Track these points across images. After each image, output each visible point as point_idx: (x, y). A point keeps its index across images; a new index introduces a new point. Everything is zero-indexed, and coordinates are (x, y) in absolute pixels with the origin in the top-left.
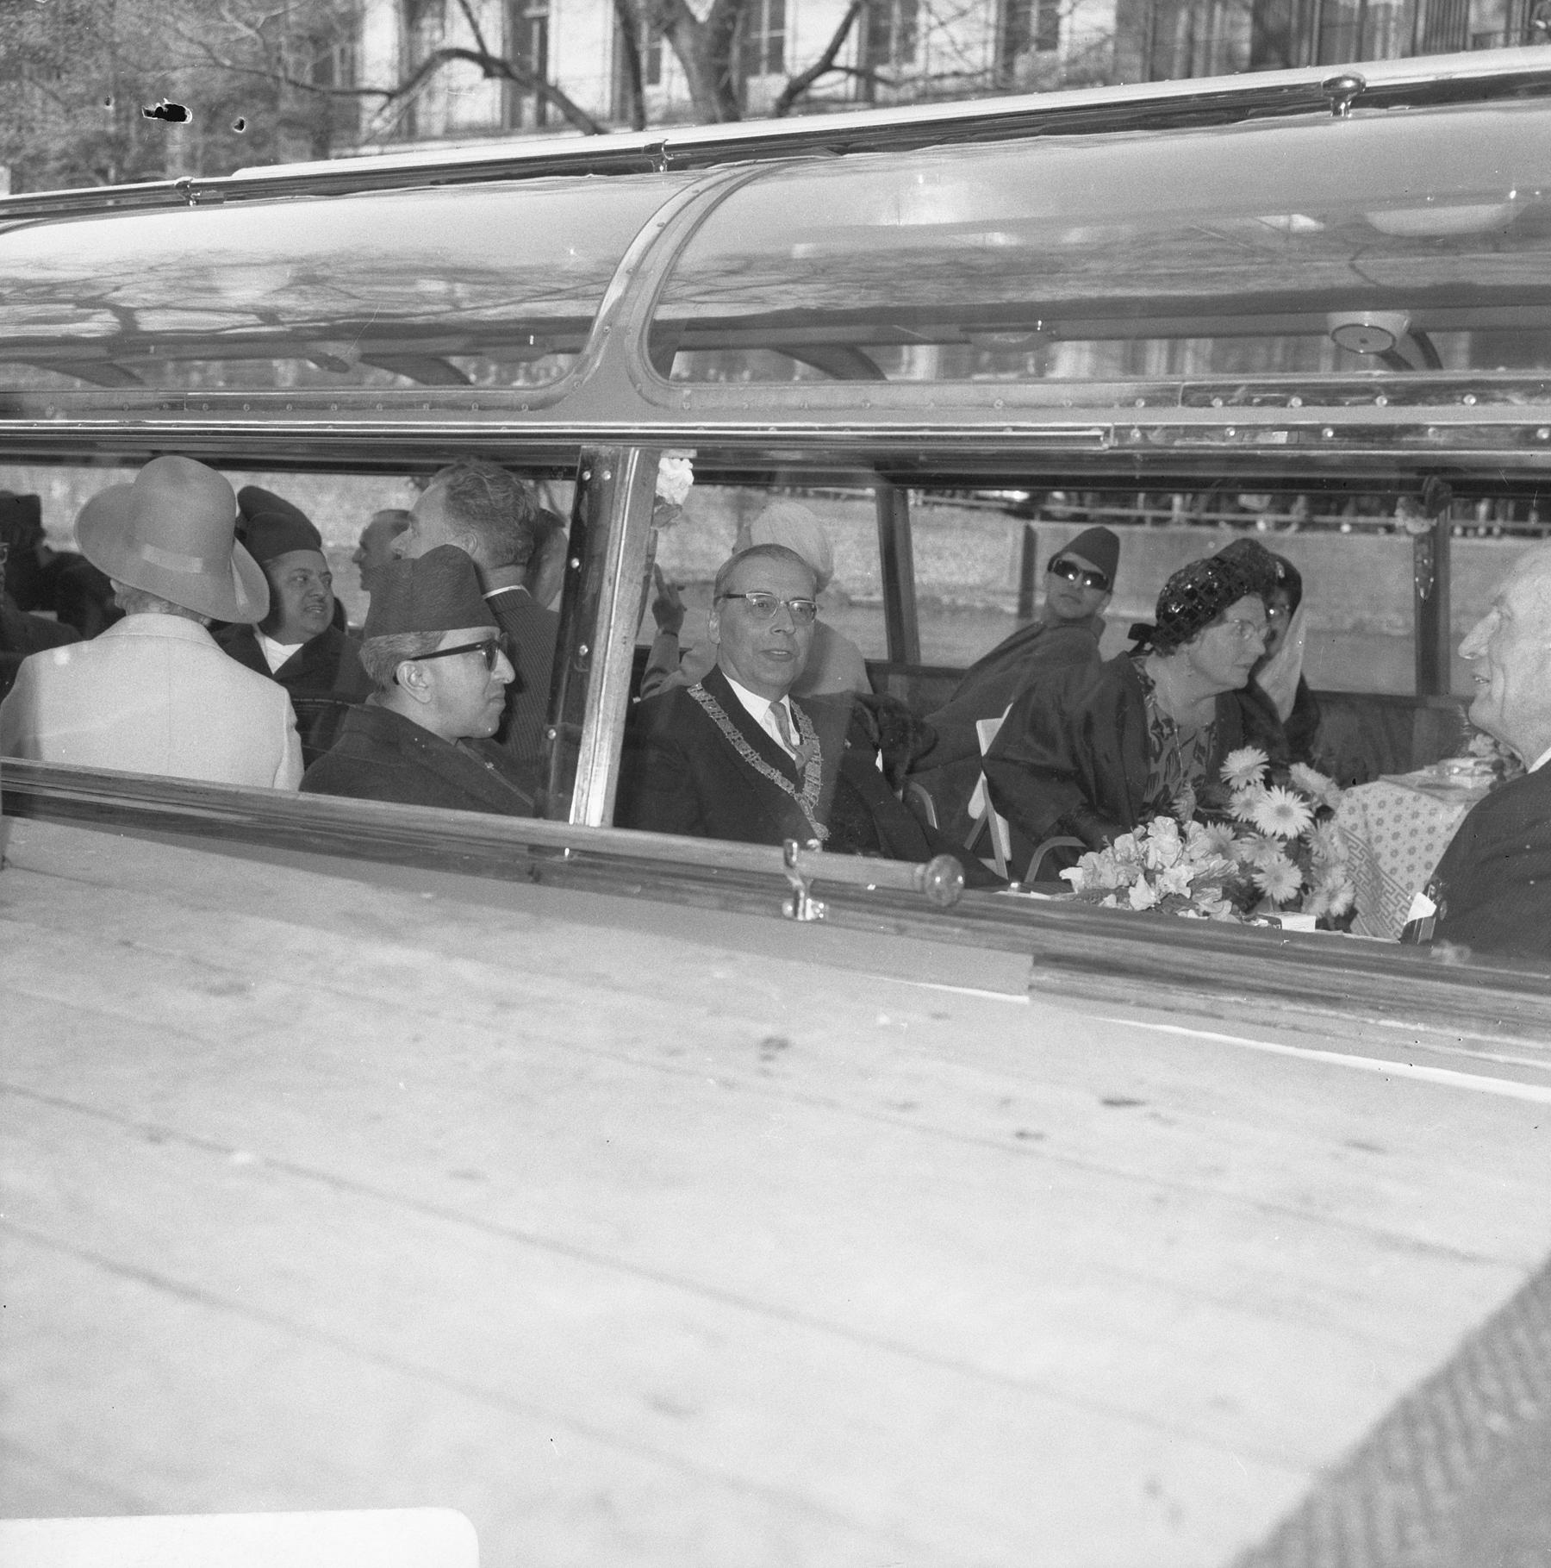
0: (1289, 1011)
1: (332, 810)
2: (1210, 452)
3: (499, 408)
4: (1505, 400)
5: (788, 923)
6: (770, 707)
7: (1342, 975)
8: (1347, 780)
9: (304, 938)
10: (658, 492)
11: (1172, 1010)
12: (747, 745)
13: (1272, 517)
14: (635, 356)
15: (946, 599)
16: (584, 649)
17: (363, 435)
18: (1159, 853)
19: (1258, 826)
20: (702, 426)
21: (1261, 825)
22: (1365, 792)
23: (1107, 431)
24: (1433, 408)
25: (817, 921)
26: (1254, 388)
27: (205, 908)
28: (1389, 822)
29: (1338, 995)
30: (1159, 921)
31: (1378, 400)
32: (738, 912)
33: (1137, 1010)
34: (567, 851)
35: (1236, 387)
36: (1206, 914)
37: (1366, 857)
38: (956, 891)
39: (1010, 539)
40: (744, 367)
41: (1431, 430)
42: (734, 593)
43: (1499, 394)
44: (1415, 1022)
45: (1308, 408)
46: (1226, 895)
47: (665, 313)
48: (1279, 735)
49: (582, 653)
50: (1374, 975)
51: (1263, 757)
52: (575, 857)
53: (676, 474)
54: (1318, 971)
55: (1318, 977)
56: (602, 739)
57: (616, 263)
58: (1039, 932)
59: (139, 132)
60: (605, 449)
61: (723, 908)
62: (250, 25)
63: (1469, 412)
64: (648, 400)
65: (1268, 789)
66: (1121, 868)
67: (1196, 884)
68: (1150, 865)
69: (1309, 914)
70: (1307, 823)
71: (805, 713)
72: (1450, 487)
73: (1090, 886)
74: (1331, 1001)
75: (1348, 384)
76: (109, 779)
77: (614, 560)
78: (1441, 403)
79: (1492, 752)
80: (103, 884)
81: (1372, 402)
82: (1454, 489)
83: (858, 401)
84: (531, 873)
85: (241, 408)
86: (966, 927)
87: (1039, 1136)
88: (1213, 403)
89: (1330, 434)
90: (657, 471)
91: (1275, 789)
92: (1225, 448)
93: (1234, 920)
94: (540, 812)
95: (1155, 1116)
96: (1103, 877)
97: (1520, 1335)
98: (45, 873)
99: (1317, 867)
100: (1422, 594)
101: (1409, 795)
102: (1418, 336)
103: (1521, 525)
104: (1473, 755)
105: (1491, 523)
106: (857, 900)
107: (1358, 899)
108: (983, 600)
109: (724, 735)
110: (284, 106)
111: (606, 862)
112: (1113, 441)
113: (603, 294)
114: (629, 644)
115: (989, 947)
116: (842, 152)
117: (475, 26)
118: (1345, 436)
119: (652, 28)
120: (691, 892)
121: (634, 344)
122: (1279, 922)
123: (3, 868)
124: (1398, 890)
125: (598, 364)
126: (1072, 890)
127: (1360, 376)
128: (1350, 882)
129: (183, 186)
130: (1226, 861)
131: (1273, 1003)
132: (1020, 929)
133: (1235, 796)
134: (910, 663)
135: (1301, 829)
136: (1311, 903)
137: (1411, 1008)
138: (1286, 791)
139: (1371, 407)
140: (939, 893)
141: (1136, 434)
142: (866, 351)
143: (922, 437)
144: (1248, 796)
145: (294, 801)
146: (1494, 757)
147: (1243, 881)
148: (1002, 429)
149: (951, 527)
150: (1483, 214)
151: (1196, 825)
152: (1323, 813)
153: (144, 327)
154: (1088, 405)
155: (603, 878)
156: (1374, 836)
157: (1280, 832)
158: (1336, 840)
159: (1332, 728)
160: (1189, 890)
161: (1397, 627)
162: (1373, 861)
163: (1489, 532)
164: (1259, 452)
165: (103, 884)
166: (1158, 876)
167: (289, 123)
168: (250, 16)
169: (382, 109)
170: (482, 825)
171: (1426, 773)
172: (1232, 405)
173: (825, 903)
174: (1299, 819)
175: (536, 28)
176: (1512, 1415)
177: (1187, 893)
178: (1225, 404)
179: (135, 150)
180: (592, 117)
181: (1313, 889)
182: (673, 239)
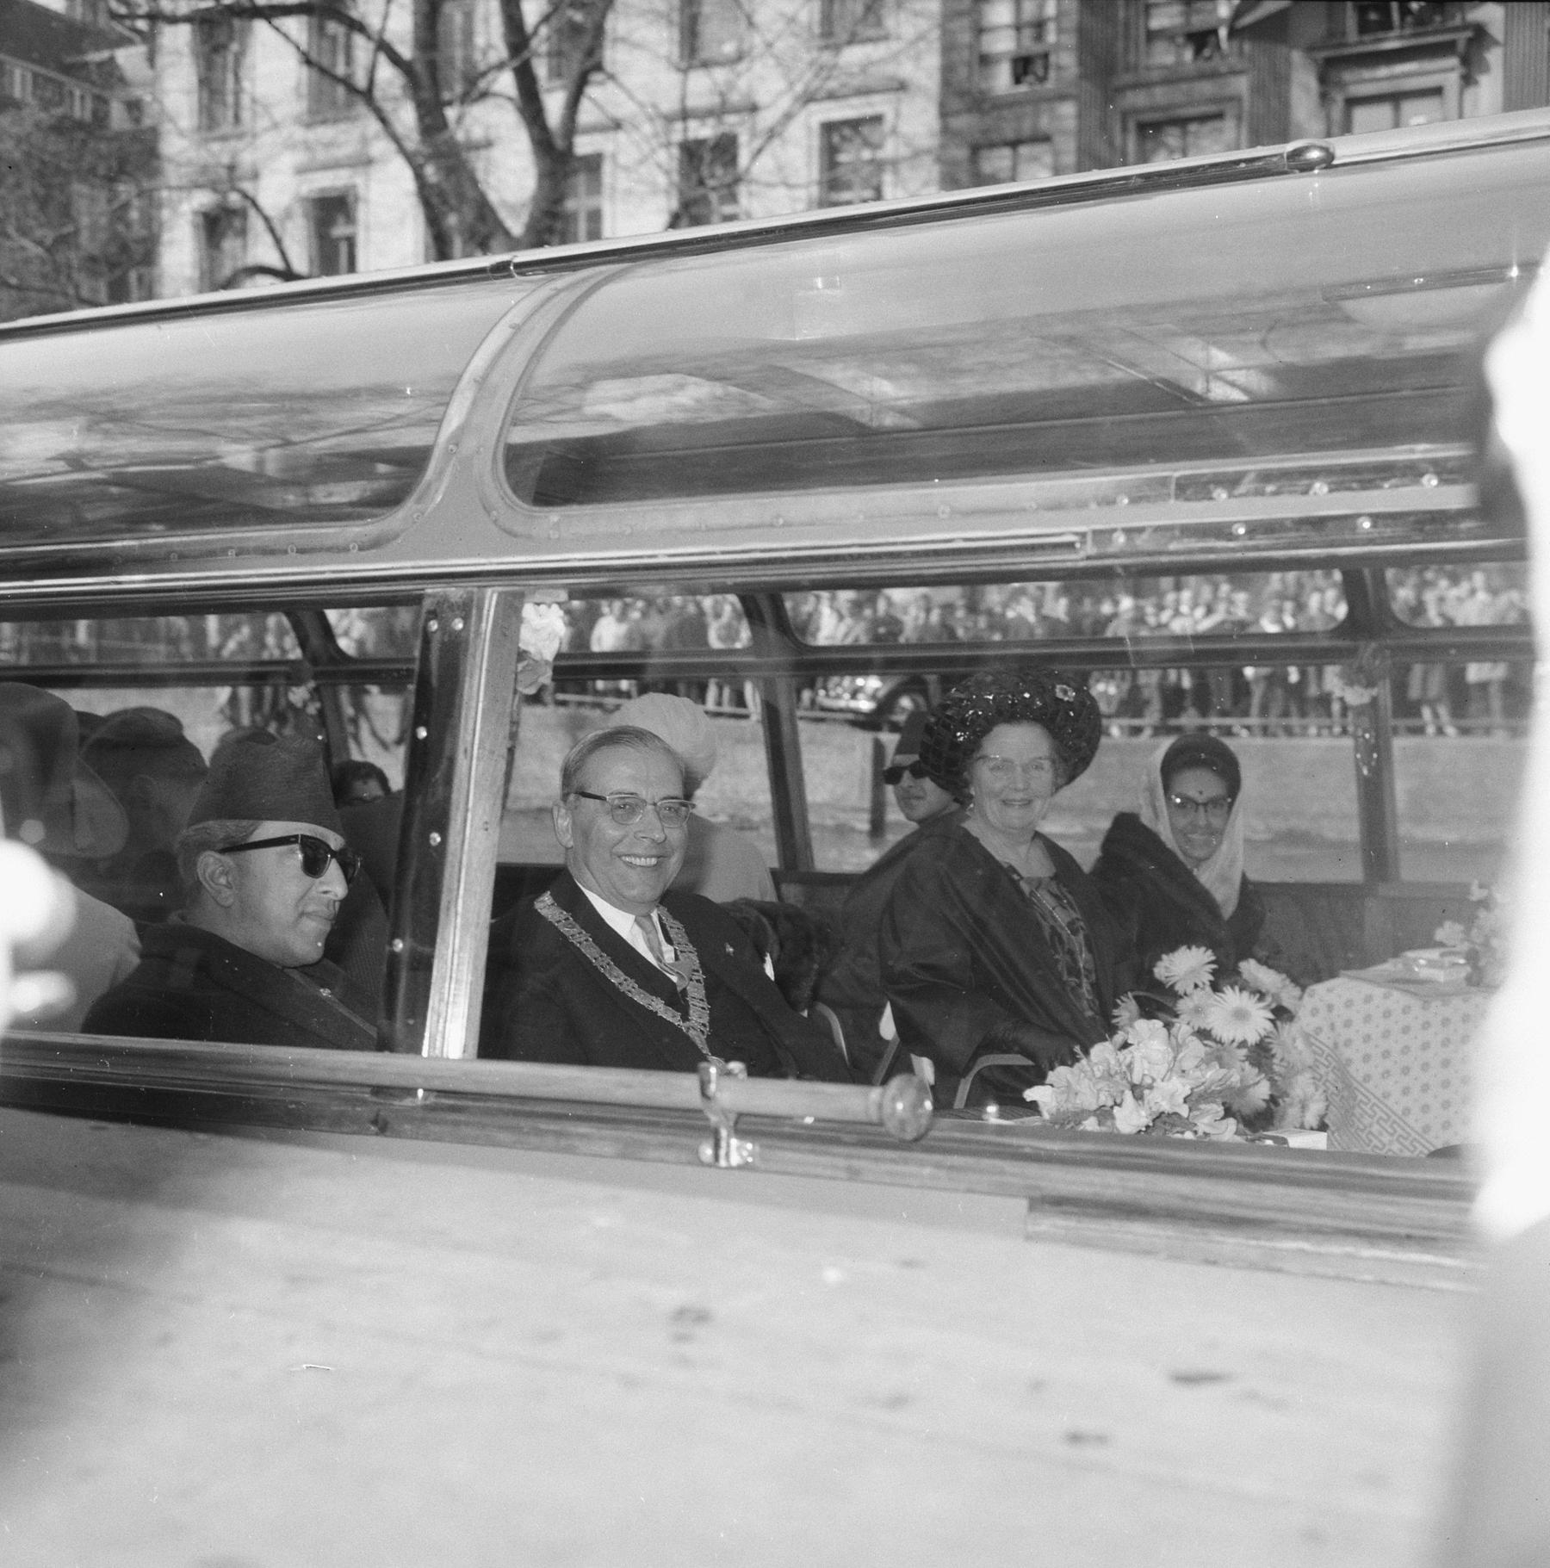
2: (1212, 557)
3: (321, 550)
5: (707, 1170)
8: (1306, 974)
10: (522, 646)
11: (1214, 1263)
12: (617, 971)
13: (1127, 722)
14: (488, 478)
16: (436, 838)
18: (1146, 1065)
22: (1329, 991)
23: (1083, 535)
25: (744, 1167)
29: (1435, 1234)
31: (1425, 479)
34: (420, 1093)
38: (924, 1121)
39: (858, 754)
42: (591, 791)
45: (1336, 495)
47: (519, 436)
49: (433, 843)
51: (1209, 956)
52: (432, 1100)
57: (459, 377)
58: (1033, 1169)
60: (455, 592)
61: (623, 1156)
62: (40, 243)
64: (505, 531)
66: (1102, 1085)
67: (1191, 1100)
68: (1136, 1080)
70: (1269, 1026)
75: (1384, 462)
77: (471, 726)
79: (1462, 940)
83: (767, 519)
84: (375, 1122)
86: (938, 1166)
88: (1215, 495)
90: (520, 620)
92: (1233, 550)
94: (384, 1044)
99: (1280, 1075)
100: (1365, 772)
101: (1378, 992)
104: (1441, 945)
106: (792, 1137)
117: (278, 242)
119: (465, 243)
120: (583, 1136)
122: (1285, 1141)
124: (1374, 1100)
125: (439, 498)
130: (1224, 1071)
134: (803, 869)
135: (1263, 1033)
140: (902, 1123)
141: (1120, 539)
146: (1465, 947)
152: (1281, 1014)
154: (1057, 506)
155: (467, 1124)
156: (1341, 1041)
157: (1239, 1039)
158: (1300, 1044)
160: (1186, 1107)
162: (1342, 1069)
166: (1146, 1092)
168: (39, 233)
171: (1390, 967)
172: (1241, 495)
173: (753, 1143)
174: (1258, 1023)
175: (343, 248)
177: (1184, 1111)
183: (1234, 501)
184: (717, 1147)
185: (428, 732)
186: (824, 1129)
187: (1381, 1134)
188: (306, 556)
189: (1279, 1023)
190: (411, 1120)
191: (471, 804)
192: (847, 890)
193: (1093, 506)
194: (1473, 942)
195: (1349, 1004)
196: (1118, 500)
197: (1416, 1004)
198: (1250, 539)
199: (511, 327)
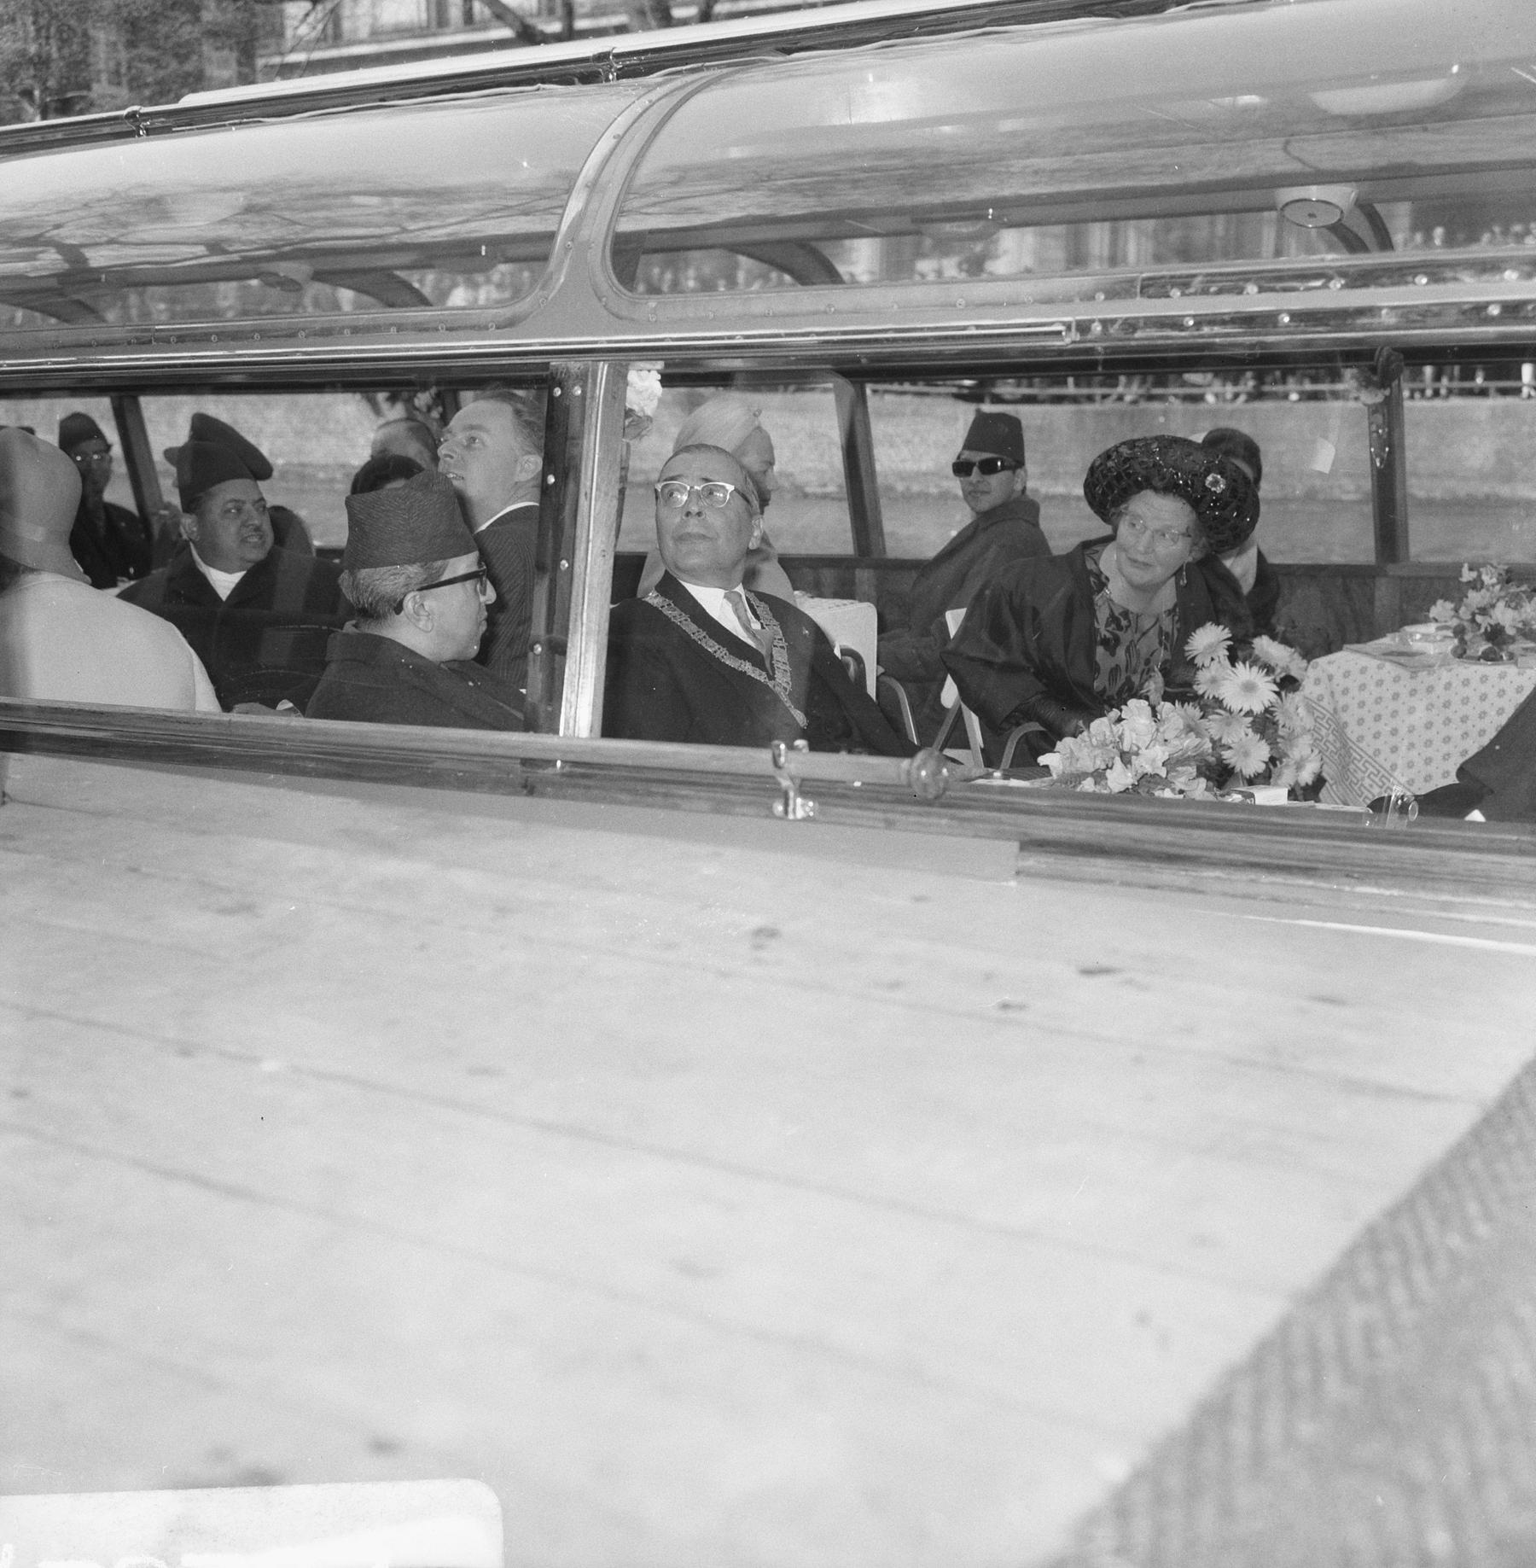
0: (1267, 882)
1: (326, 734)
2: (1170, 342)
4: (1456, 279)
5: (779, 822)
6: (726, 597)
7: (1318, 847)
9: (304, 856)
10: (628, 406)
11: (1154, 887)
12: (712, 642)
15: (900, 487)
17: (333, 361)
18: (1134, 735)
19: (1225, 703)
20: (668, 337)
21: (1228, 702)
23: (1068, 326)
24: (1386, 290)
25: (807, 819)
26: (1211, 278)
27: (204, 833)
28: (1354, 692)
29: (1314, 865)
30: (1138, 802)
32: (729, 814)
33: (1122, 889)
34: (559, 764)
35: (1194, 276)
36: (1181, 792)
37: (1333, 726)
40: (687, 266)
41: (1384, 312)
43: (1449, 274)
44: (1388, 887)
45: (1264, 295)
46: (1200, 774)
47: (627, 225)
48: (1244, 611)
50: (1348, 844)
51: (1227, 633)
52: (567, 769)
53: (645, 385)
54: (1292, 843)
55: (1295, 849)
56: (586, 651)
58: (1022, 819)
59: (60, 49)
60: (575, 365)
63: (1420, 293)
65: (1233, 665)
66: (1097, 752)
68: (1126, 749)
69: (1276, 785)
70: (1274, 697)
71: (761, 600)
72: (1402, 356)
73: (1068, 771)
74: (1307, 871)
76: (102, 713)
77: (590, 473)
78: (1394, 284)
80: (103, 814)
81: (1325, 286)
82: (1406, 358)
83: (822, 308)
84: (525, 786)
85: (209, 340)
86: (953, 818)
87: (1022, 1007)
88: (1171, 294)
89: (1286, 319)
90: (626, 384)
91: (1240, 665)
93: (1209, 797)
95: (1130, 982)
96: (1081, 761)
97: (1475, 1164)
98: (47, 806)
99: (1282, 737)
100: (1378, 464)
101: (1374, 663)
102: (1366, 208)
103: (1467, 385)
105: (1437, 385)
106: (843, 796)
107: (1325, 767)
108: (937, 486)
109: (689, 636)
110: (207, 16)
111: (596, 771)
112: (1075, 336)
113: (564, 207)
114: (607, 557)
115: (975, 836)
116: (789, 52)
118: (1301, 321)
120: (683, 797)
121: (598, 258)
122: (1252, 796)
123: (4, 803)
125: (562, 280)
126: (1051, 775)
127: (1314, 261)
128: (1316, 751)
129: (132, 115)
130: (1198, 740)
131: (1253, 876)
132: (1004, 816)
133: (1200, 672)
134: (875, 556)
135: (1267, 704)
136: (1280, 775)
137: (1386, 874)
138: (1251, 667)
139: (1326, 291)
140: (925, 786)
142: (814, 244)
143: (887, 340)
144: (1213, 673)
145: (287, 726)
146: (1454, 622)
147: (1212, 760)
148: (965, 328)
149: (903, 415)
150: (1425, 91)
151: (1168, 705)
152: (1288, 684)
153: (93, 264)
154: (1049, 301)
157: (1246, 709)
159: (1295, 606)
160: (1164, 770)
161: (1349, 492)
162: (1340, 730)
163: (1436, 393)
164: (1217, 340)
165: (103, 814)
166: (1134, 757)
167: (213, 34)
169: (307, 15)
170: (475, 742)
171: (1389, 641)
172: (1191, 294)
174: (1264, 693)
176: (1469, 1236)
177: (1163, 772)
178: (1183, 294)
179: (57, 67)
180: (521, 13)
181: (1281, 763)
182: (630, 151)
183: (1185, 298)
184: (786, 805)
185: (556, 478)
186: (870, 791)
187: (1371, 786)
188: (454, 333)
189: (1283, 693)
190: (553, 784)
191: (591, 537)
192: (914, 574)
193: (1077, 300)
194: (1462, 619)
195: (1347, 674)
196: (1096, 297)
197: (1405, 674)
198: (1198, 330)
199: (614, 137)
